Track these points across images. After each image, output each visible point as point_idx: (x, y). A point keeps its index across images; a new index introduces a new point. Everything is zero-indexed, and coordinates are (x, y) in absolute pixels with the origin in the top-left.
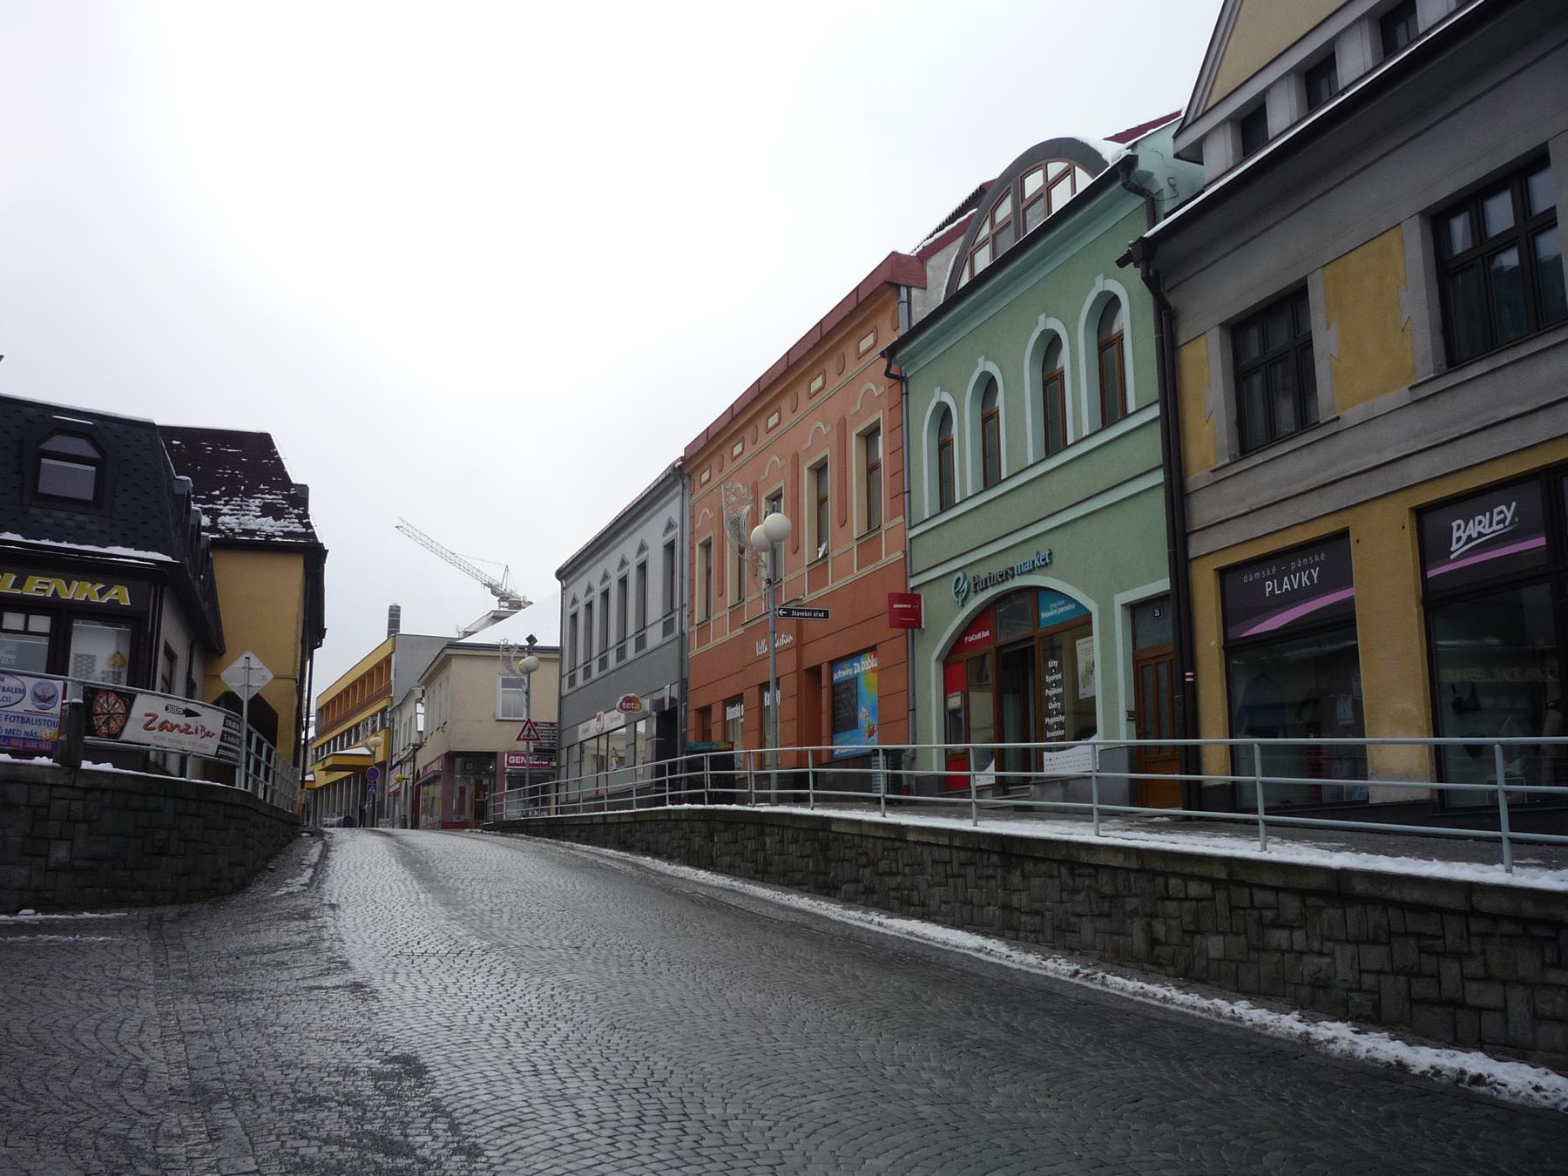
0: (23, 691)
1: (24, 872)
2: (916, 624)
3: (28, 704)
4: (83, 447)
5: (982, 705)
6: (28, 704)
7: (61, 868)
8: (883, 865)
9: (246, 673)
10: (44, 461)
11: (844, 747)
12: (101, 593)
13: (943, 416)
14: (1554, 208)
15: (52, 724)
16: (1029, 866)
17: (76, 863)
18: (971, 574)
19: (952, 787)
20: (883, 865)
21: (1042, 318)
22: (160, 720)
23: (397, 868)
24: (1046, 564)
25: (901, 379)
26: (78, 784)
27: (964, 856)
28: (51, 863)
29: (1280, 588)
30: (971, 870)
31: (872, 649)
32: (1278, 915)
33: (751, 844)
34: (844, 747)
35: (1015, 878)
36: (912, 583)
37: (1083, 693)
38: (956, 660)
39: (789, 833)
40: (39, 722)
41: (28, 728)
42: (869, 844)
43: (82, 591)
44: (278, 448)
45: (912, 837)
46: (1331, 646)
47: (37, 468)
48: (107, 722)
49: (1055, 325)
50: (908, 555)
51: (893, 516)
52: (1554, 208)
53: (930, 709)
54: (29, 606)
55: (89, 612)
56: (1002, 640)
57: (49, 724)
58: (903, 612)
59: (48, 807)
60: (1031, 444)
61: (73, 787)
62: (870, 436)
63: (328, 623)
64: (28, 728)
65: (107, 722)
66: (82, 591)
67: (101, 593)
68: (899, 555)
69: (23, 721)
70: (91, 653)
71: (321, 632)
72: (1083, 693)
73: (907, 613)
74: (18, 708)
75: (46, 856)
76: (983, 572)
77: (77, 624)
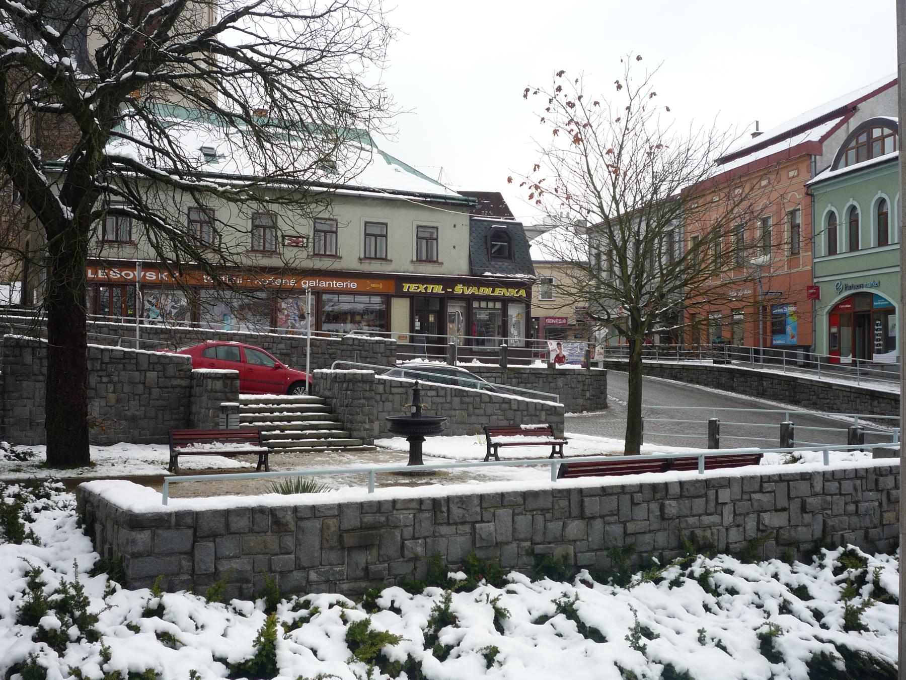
2: (818, 298)
5: (846, 333)
8: (821, 396)
11: (779, 341)
13: (831, 215)
16: (880, 400)
18: (844, 283)
19: (831, 364)
20: (821, 396)
21: (879, 192)
24: (878, 285)
25: (812, 195)
27: (855, 395)
30: (858, 400)
31: (795, 304)
32: (488, 440)
33: (755, 384)
34: (779, 341)
35: (875, 403)
36: (815, 280)
37: (890, 334)
38: (835, 315)
39: (776, 381)
42: (816, 388)
43: (511, 293)
44: (505, 200)
45: (834, 387)
49: (884, 196)
50: (813, 270)
51: (806, 251)
55: (513, 300)
56: (857, 309)
58: (813, 294)
60: (873, 241)
62: (793, 213)
66: (511, 293)
68: (809, 268)
72: (890, 334)
73: (814, 293)
76: (850, 283)
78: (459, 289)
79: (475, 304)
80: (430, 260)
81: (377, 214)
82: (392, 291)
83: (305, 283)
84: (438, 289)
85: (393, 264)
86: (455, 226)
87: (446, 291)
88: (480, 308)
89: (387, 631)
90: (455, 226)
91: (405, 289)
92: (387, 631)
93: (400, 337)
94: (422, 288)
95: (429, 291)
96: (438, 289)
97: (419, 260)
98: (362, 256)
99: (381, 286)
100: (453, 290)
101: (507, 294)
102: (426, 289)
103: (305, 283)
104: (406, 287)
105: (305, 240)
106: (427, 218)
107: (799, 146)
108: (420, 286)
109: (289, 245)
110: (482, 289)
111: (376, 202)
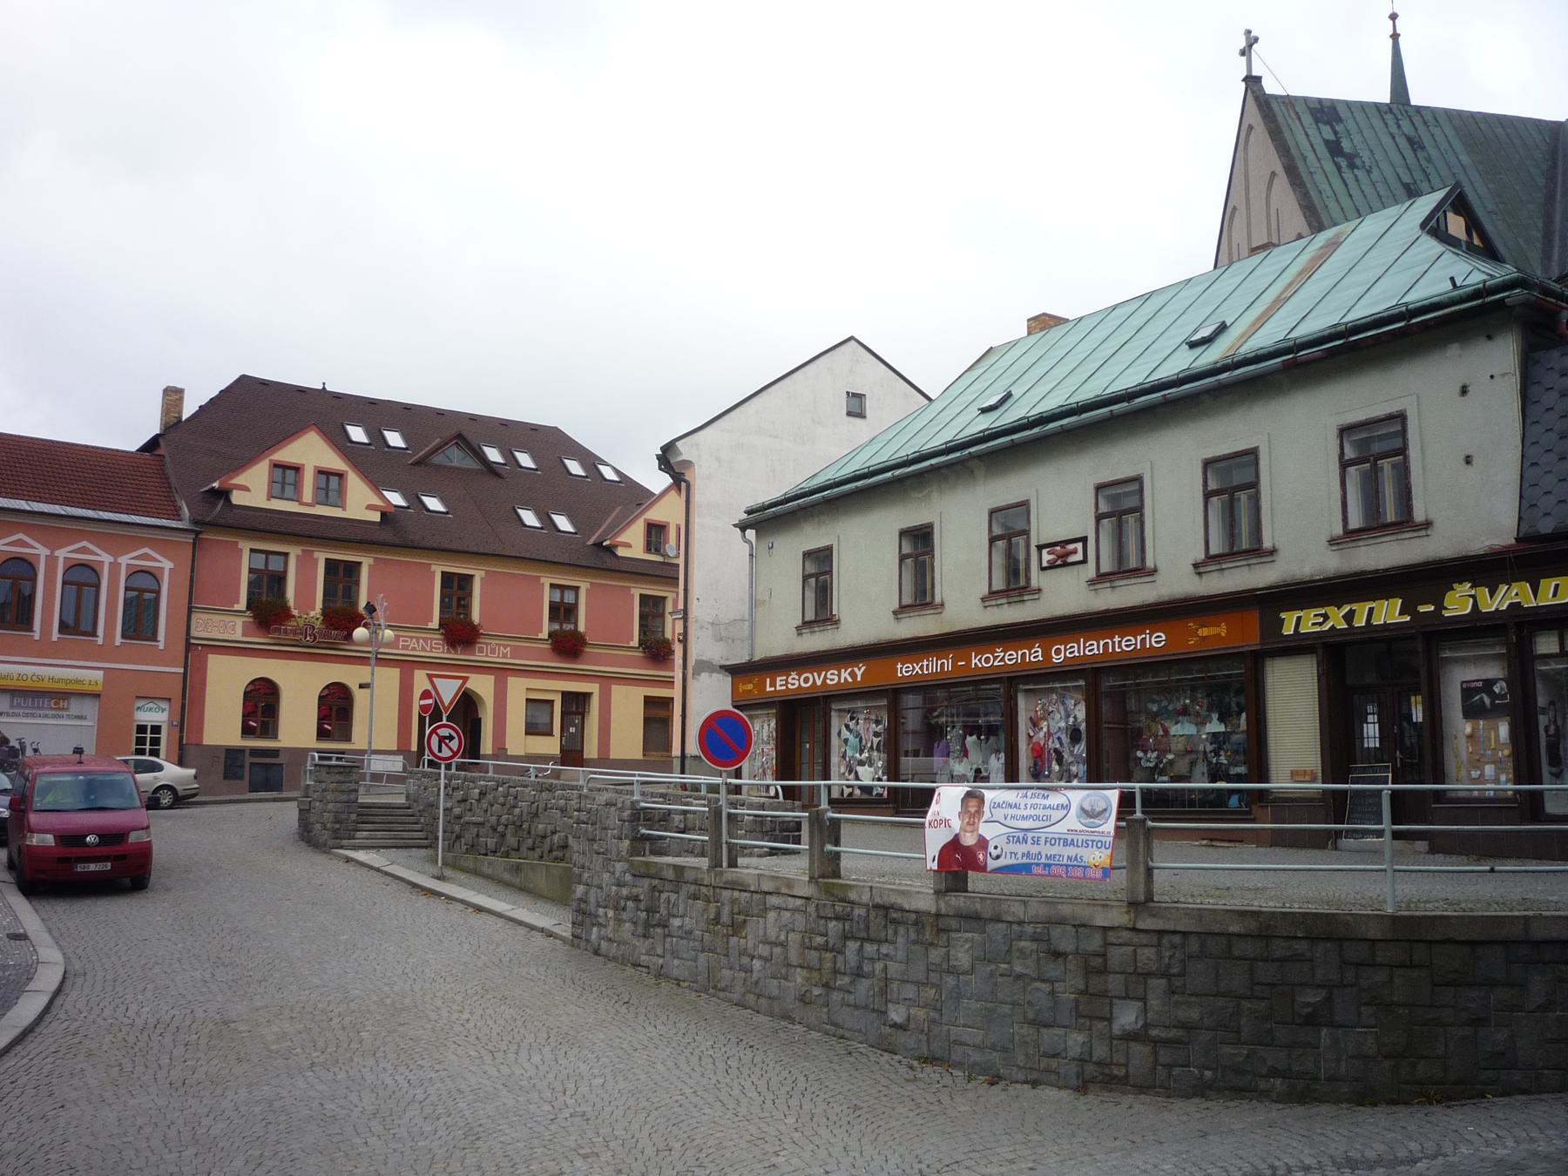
0: (1067, 807)
1: (1081, 1038)
3: (1073, 822)
6: (1073, 822)
7: (1130, 1037)
15: (1103, 845)
17: (1154, 1032)
26: (1140, 925)
28: (1116, 1030)
29: (1024, 655)
32: (1105, 962)
40: (1086, 844)
41: (1071, 851)
46: (558, 778)
57: (1100, 845)
59: (1104, 955)
61: (1134, 929)
64: (1071, 851)
69: (1066, 843)
74: (1061, 828)
75: (1110, 1020)
78: (1459, 601)
80: (1406, 523)
82: (1252, 642)
84: (1388, 612)
85: (1281, 557)
86: (1464, 391)
87: (1416, 615)
90: (1464, 391)
91: (1288, 630)
93: (1294, 775)
94: (1336, 618)
95: (1360, 622)
96: (1388, 612)
97: (1351, 535)
98: (1338, 530)
100: (1440, 606)
101: (1530, 602)
102: (1349, 617)
103: (1058, 652)
104: (1290, 622)
105: (1079, 546)
108: (1331, 610)
109: (1052, 566)
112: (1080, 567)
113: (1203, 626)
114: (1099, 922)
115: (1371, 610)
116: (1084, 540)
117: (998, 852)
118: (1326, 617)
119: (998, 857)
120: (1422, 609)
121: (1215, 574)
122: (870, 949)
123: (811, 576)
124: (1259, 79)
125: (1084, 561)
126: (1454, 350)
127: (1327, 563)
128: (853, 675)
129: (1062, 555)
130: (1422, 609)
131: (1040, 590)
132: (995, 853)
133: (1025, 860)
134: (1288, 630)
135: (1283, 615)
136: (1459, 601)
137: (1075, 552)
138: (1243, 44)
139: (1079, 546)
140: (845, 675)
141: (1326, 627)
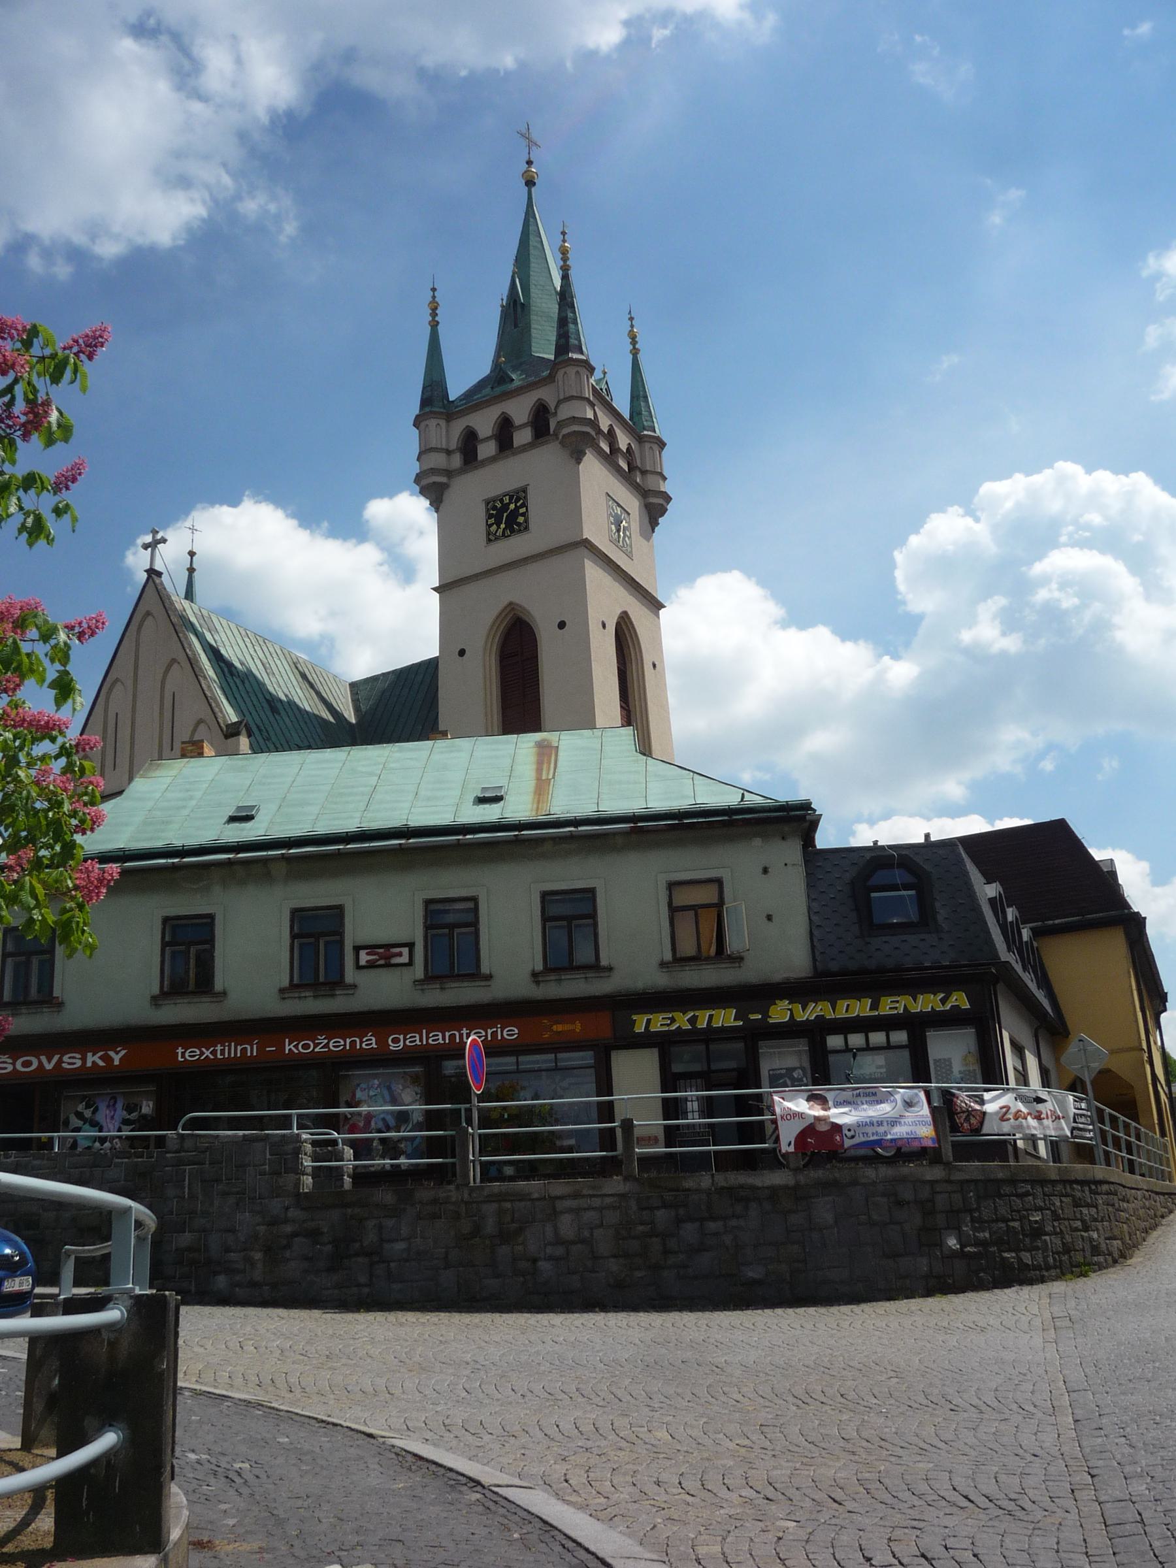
1: (925, 1261)
4: (898, 876)
9: (1090, 1049)
10: (873, 895)
12: (943, 1001)
14: (524, 490)
15: (926, 1123)
22: (1013, 1110)
23: (181, 1335)
43: (926, 1003)
47: (869, 899)
48: (967, 1119)
52: (524, 490)
53: (418, 1165)
54: (887, 1024)
61: (949, 1181)
63: (1167, 986)
65: (967, 1119)
66: (926, 1003)
67: (943, 1001)
70: (946, 1057)
71: (1163, 998)
77: (930, 1034)
78: (780, 1012)
79: (834, 1041)
81: (569, 874)
83: (396, 1041)
84: (725, 1018)
86: (765, 871)
88: (847, 1049)
89: (876, 842)
90: (765, 871)
91: (640, 1028)
92: (876, 842)
94: (682, 1021)
95: (702, 1024)
96: (725, 1018)
98: (539, 967)
99: (578, 1027)
100: (766, 1015)
101: (830, 1015)
102: (693, 1020)
104: (640, 1023)
105: (405, 951)
106: (691, 863)
107: (982, 913)
108: (678, 1015)
109: (371, 965)
110: (842, 1004)
111: (196, 669)
112: (404, 969)
113: (557, 1023)
114: (928, 1178)
115: (711, 1017)
116: (411, 946)
117: (852, 1133)
118: (673, 1020)
119: (853, 1137)
120: (752, 1017)
121: (297, 1001)
122: (712, 1226)
123: (11, 955)
124: (159, 574)
125: (410, 963)
126: (757, 842)
127: (661, 980)
128: (214, 1053)
129: (384, 955)
130: (752, 1017)
131: (741, 959)
132: (849, 1134)
133: (875, 1138)
134: (640, 1028)
135: (634, 1017)
136: (780, 1012)
137: (400, 955)
138: (78, 525)
139: (405, 951)
140: (91, 1059)
141: (674, 1028)
